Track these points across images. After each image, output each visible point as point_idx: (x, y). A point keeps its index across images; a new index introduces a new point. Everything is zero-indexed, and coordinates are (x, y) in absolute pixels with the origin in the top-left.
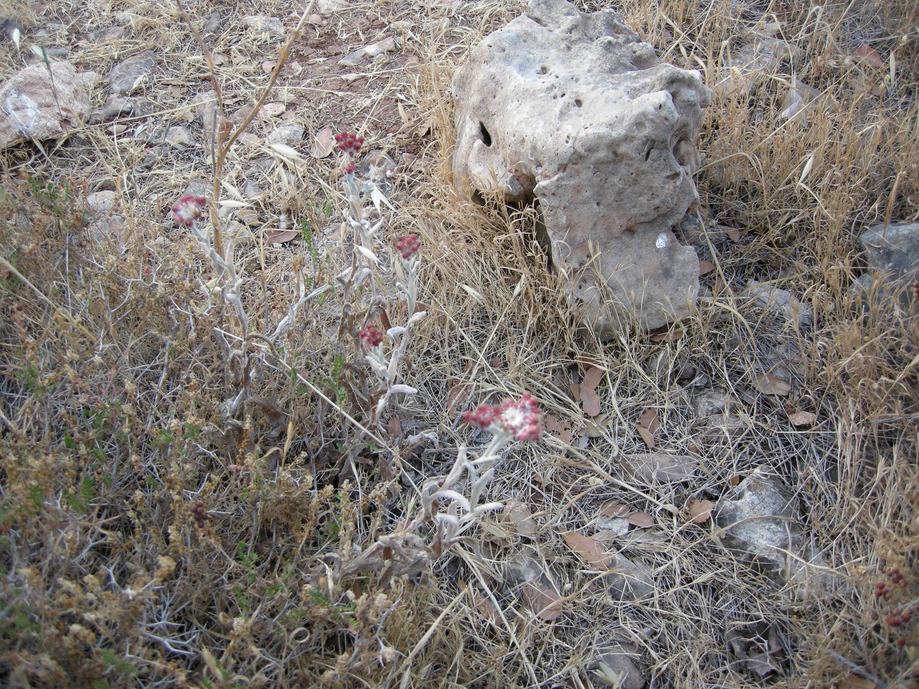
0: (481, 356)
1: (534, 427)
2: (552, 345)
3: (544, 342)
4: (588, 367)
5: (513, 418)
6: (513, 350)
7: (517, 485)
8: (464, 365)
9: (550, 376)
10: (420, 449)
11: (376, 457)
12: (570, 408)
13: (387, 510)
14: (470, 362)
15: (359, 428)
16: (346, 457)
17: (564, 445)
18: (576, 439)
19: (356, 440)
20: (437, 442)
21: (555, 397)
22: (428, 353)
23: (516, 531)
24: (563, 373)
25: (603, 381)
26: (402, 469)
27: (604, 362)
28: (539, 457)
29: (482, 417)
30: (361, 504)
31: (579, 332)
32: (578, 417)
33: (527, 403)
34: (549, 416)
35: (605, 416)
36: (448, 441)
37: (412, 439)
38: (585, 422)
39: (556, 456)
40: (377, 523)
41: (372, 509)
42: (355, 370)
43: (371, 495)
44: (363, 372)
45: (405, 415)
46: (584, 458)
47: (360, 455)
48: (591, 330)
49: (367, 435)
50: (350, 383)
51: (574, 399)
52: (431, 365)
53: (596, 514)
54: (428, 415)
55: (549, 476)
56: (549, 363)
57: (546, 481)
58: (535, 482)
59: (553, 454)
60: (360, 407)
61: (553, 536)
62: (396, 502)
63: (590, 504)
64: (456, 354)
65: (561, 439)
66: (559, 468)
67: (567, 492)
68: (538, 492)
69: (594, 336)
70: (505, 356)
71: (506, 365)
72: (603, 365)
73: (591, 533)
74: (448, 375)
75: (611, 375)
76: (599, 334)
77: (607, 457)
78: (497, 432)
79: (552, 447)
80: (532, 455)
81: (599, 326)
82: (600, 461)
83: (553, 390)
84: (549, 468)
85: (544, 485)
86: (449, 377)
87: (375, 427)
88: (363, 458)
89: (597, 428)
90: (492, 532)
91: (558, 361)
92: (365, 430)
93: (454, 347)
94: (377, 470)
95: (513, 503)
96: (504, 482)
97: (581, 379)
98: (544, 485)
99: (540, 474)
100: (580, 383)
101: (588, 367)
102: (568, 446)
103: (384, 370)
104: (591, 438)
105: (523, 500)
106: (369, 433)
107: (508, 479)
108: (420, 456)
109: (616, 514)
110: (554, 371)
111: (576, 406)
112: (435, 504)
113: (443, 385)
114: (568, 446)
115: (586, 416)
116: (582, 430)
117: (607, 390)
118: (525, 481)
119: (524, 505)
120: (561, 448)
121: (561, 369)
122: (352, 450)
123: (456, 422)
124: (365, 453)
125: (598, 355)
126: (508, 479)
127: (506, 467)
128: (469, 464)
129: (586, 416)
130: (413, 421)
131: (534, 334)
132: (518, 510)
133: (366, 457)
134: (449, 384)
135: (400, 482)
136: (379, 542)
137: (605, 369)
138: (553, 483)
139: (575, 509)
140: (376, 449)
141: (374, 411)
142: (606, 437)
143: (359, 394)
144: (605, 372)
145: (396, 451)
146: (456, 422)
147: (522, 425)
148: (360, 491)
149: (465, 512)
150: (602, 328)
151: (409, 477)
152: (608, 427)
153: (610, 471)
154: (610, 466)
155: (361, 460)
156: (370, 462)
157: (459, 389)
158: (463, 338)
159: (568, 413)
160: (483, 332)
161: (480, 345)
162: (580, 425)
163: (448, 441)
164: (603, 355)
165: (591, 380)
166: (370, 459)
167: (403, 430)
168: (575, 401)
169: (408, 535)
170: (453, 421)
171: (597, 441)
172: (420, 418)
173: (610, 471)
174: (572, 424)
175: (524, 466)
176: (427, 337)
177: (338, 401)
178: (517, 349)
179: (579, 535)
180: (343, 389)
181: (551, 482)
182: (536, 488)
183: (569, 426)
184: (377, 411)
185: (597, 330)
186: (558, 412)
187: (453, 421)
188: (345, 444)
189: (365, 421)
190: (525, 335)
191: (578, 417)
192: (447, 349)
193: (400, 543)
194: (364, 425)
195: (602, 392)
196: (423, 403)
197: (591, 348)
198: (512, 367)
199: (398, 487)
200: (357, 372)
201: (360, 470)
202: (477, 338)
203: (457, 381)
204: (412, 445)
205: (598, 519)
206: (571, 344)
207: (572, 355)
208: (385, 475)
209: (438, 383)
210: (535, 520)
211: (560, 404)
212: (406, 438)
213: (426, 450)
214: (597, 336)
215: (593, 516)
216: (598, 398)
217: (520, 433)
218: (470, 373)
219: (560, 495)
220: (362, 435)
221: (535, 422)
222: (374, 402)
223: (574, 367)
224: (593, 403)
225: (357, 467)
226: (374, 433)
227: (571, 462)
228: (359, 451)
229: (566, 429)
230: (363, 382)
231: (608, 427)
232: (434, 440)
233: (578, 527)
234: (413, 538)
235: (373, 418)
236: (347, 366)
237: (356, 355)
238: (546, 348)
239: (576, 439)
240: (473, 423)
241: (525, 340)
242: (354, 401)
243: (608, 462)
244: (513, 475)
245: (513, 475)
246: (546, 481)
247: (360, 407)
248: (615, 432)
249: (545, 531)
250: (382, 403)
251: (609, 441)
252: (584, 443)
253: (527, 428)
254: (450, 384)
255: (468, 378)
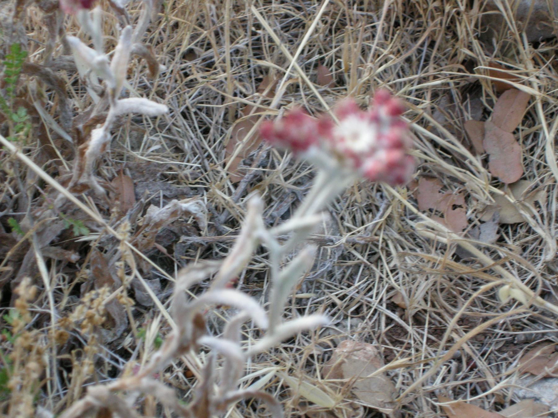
0: (293, 61)
1: (396, 155)
2: (432, 45)
3: (416, 40)
4: (501, 90)
5: (355, 136)
6: (357, 51)
7: (357, 311)
8: (260, 78)
9: (427, 102)
10: (171, 236)
11: (84, 249)
12: (463, 166)
13: (106, 349)
14: (272, 72)
15: (54, 190)
16: (27, 245)
17: (448, 235)
18: (473, 227)
19: (48, 215)
20: (204, 223)
21: (435, 145)
22: (190, 54)
23: (354, 396)
24: (451, 100)
25: (530, 117)
26: (135, 272)
27: (533, 79)
28: (401, 256)
29: (295, 132)
30: (54, 334)
31: (486, 20)
32: (479, 184)
33: (383, 112)
34: (422, 181)
35: (530, 184)
36: (226, 223)
37: (156, 213)
38: (492, 194)
39: (435, 256)
40: (84, 368)
41: (73, 345)
42: (46, 77)
43: (74, 317)
44: (62, 84)
45: (144, 172)
46: (488, 260)
47: (52, 244)
48: (508, 16)
49: (68, 200)
50: (37, 105)
51: (471, 149)
52: (198, 76)
53: (511, 369)
54: (188, 172)
55: (420, 294)
56: (425, 79)
57: (415, 304)
58: (393, 307)
59: (429, 252)
60: (55, 150)
61: (426, 409)
62: (122, 337)
63: (499, 351)
64: (246, 57)
65: (446, 225)
66: (440, 280)
67: (452, 323)
68: (398, 326)
69: (513, 28)
70: (339, 65)
71: (341, 82)
72: (530, 84)
73: (499, 406)
74: (229, 96)
75: (545, 104)
76: (525, 25)
77: (534, 260)
78: (322, 165)
79: (428, 240)
80: (388, 254)
81: (525, 9)
82: (520, 270)
83: (433, 130)
84: (420, 279)
85: (410, 312)
86: (232, 101)
87: (85, 187)
88: (59, 250)
89: (515, 207)
90: (310, 398)
91: (442, 76)
92: (64, 192)
93: (241, 45)
94: (85, 273)
95: (349, 345)
96: (334, 305)
97: (486, 113)
98: (410, 312)
99: (402, 290)
100: (484, 119)
101: (501, 90)
102: (457, 237)
103: (102, 64)
104: (504, 226)
105: (369, 340)
106: (72, 197)
107: (342, 298)
108: (170, 250)
109: (548, 370)
110: (435, 95)
111: (477, 162)
112: (200, 324)
113: (219, 117)
114: (457, 237)
115: (496, 182)
116: (486, 209)
117: (536, 135)
118: (375, 303)
119: (370, 348)
120: (444, 240)
121: (448, 92)
122: (39, 234)
123: (242, 186)
124: (65, 240)
125: (521, 67)
126: (342, 298)
127: (338, 274)
128: (268, 237)
129: (496, 182)
130: (159, 183)
131: (397, 24)
132: (359, 356)
133: (67, 248)
134: (230, 117)
135: (131, 293)
136: (89, 398)
137: (534, 91)
138: (428, 307)
139: (470, 359)
140: (85, 231)
141: (82, 153)
142: (532, 223)
143: (55, 126)
144: (533, 98)
145: (122, 232)
146: (242, 186)
147: (373, 151)
148: (52, 312)
149: (258, 334)
150: (529, 14)
151: (149, 289)
152: (537, 204)
153: (540, 288)
154: (540, 279)
155: (56, 253)
156: (74, 257)
157: (249, 124)
158: (258, 26)
159: (460, 176)
160: (298, 16)
161: (292, 42)
162: (482, 198)
163: (226, 223)
164: (530, 66)
165: (506, 114)
166: (75, 256)
167: (137, 200)
168: (474, 154)
169: (146, 382)
170: (236, 185)
171: (515, 232)
172: (174, 177)
173: (540, 288)
174: (467, 197)
175: (372, 275)
176: (188, 23)
177: (13, 135)
178: (364, 52)
179: (476, 410)
180: (23, 111)
181: (424, 306)
182: (395, 316)
183: (461, 202)
184: (88, 152)
185: (520, 17)
186: (441, 174)
187: (236, 185)
188: (26, 222)
189: (64, 177)
190: (380, 24)
191: (479, 184)
192: (228, 48)
193: (130, 401)
194: (64, 184)
195: (526, 138)
196: (178, 150)
197: (508, 51)
198: (354, 85)
199: (129, 304)
200: (49, 81)
201: (54, 269)
202: (286, 28)
203: (246, 107)
204: (157, 225)
205: (514, 379)
206: (468, 44)
207: (470, 64)
208: (101, 278)
209: (209, 112)
210: (391, 377)
211: (445, 158)
212: (145, 213)
213: (183, 238)
214: (520, 29)
215: (504, 373)
216: (519, 149)
217: (369, 165)
218: (272, 93)
219: (438, 332)
220: (58, 203)
221: (398, 145)
222: (81, 138)
223: (473, 89)
224: (509, 159)
225: (48, 265)
226: (81, 199)
227: (462, 269)
228: (51, 236)
229: (455, 207)
230: (62, 103)
231: (537, 204)
232: (200, 215)
233: (474, 393)
234: (152, 389)
235: (81, 169)
236: (32, 69)
237: (49, 49)
238: (419, 51)
239: (473, 227)
240: (278, 144)
241: (379, 33)
242: (44, 139)
243: (536, 270)
244: (351, 292)
245: (351, 292)
246: (415, 304)
247: (55, 150)
248: (550, 214)
249: (411, 399)
250: (98, 135)
251: (539, 231)
252: (489, 236)
253: (383, 156)
254: (232, 115)
255: (267, 103)
